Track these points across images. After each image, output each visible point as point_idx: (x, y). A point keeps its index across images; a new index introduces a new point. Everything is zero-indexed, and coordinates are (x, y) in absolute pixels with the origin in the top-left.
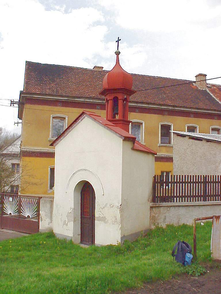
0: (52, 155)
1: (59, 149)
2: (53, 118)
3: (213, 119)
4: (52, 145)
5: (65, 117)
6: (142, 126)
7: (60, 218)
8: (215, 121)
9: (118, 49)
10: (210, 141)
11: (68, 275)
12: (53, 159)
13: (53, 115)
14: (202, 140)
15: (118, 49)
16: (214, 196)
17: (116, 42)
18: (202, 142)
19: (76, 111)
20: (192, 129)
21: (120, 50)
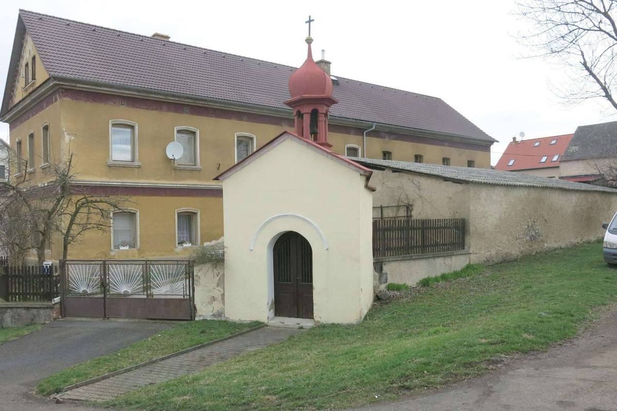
0: (218, 193)
1: (229, 186)
2: (179, 131)
3: (348, 133)
4: (217, 179)
5: (133, 125)
6: (252, 143)
7: (247, 290)
8: (245, 124)
9: (309, 35)
10: (399, 172)
11: (33, 317)
12: (221, 198)
13: (113, 121)
14: (384, 170)
15: (309, 35)
16: (1, 183)
17: (306, 22)
18: (384, 171)
19: (272, 130)
20: (387, 155)
21: (312, 36)
